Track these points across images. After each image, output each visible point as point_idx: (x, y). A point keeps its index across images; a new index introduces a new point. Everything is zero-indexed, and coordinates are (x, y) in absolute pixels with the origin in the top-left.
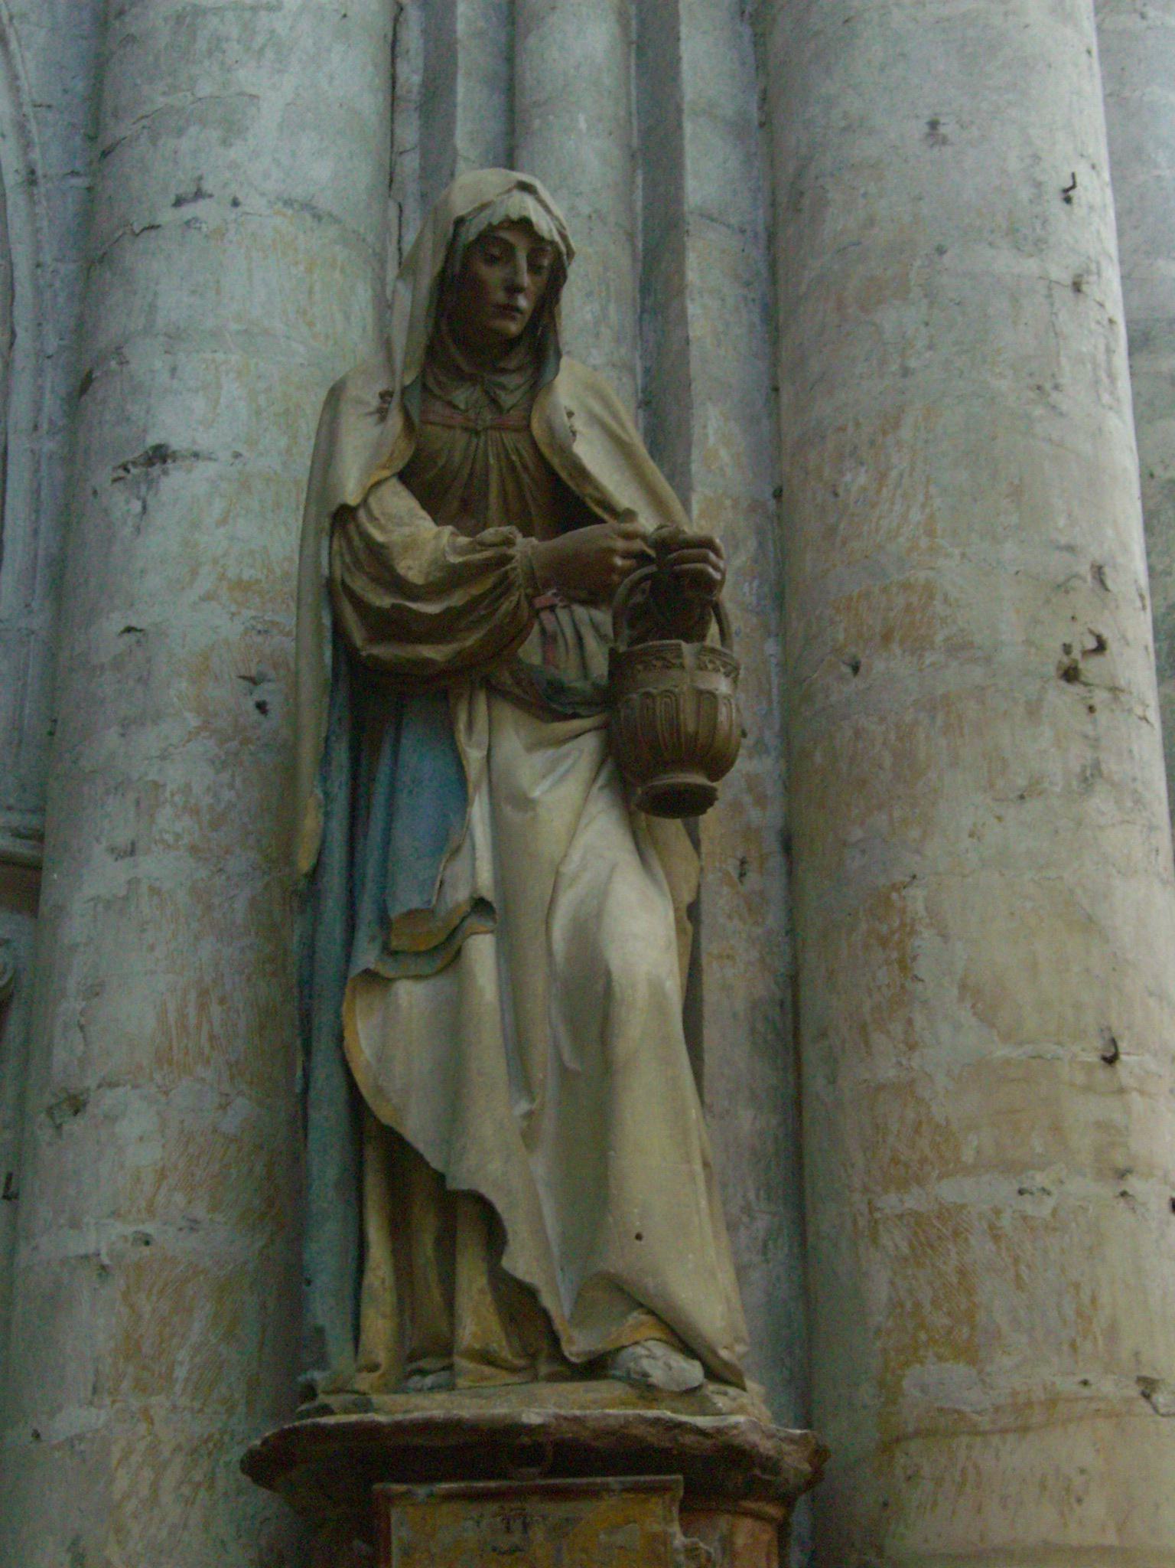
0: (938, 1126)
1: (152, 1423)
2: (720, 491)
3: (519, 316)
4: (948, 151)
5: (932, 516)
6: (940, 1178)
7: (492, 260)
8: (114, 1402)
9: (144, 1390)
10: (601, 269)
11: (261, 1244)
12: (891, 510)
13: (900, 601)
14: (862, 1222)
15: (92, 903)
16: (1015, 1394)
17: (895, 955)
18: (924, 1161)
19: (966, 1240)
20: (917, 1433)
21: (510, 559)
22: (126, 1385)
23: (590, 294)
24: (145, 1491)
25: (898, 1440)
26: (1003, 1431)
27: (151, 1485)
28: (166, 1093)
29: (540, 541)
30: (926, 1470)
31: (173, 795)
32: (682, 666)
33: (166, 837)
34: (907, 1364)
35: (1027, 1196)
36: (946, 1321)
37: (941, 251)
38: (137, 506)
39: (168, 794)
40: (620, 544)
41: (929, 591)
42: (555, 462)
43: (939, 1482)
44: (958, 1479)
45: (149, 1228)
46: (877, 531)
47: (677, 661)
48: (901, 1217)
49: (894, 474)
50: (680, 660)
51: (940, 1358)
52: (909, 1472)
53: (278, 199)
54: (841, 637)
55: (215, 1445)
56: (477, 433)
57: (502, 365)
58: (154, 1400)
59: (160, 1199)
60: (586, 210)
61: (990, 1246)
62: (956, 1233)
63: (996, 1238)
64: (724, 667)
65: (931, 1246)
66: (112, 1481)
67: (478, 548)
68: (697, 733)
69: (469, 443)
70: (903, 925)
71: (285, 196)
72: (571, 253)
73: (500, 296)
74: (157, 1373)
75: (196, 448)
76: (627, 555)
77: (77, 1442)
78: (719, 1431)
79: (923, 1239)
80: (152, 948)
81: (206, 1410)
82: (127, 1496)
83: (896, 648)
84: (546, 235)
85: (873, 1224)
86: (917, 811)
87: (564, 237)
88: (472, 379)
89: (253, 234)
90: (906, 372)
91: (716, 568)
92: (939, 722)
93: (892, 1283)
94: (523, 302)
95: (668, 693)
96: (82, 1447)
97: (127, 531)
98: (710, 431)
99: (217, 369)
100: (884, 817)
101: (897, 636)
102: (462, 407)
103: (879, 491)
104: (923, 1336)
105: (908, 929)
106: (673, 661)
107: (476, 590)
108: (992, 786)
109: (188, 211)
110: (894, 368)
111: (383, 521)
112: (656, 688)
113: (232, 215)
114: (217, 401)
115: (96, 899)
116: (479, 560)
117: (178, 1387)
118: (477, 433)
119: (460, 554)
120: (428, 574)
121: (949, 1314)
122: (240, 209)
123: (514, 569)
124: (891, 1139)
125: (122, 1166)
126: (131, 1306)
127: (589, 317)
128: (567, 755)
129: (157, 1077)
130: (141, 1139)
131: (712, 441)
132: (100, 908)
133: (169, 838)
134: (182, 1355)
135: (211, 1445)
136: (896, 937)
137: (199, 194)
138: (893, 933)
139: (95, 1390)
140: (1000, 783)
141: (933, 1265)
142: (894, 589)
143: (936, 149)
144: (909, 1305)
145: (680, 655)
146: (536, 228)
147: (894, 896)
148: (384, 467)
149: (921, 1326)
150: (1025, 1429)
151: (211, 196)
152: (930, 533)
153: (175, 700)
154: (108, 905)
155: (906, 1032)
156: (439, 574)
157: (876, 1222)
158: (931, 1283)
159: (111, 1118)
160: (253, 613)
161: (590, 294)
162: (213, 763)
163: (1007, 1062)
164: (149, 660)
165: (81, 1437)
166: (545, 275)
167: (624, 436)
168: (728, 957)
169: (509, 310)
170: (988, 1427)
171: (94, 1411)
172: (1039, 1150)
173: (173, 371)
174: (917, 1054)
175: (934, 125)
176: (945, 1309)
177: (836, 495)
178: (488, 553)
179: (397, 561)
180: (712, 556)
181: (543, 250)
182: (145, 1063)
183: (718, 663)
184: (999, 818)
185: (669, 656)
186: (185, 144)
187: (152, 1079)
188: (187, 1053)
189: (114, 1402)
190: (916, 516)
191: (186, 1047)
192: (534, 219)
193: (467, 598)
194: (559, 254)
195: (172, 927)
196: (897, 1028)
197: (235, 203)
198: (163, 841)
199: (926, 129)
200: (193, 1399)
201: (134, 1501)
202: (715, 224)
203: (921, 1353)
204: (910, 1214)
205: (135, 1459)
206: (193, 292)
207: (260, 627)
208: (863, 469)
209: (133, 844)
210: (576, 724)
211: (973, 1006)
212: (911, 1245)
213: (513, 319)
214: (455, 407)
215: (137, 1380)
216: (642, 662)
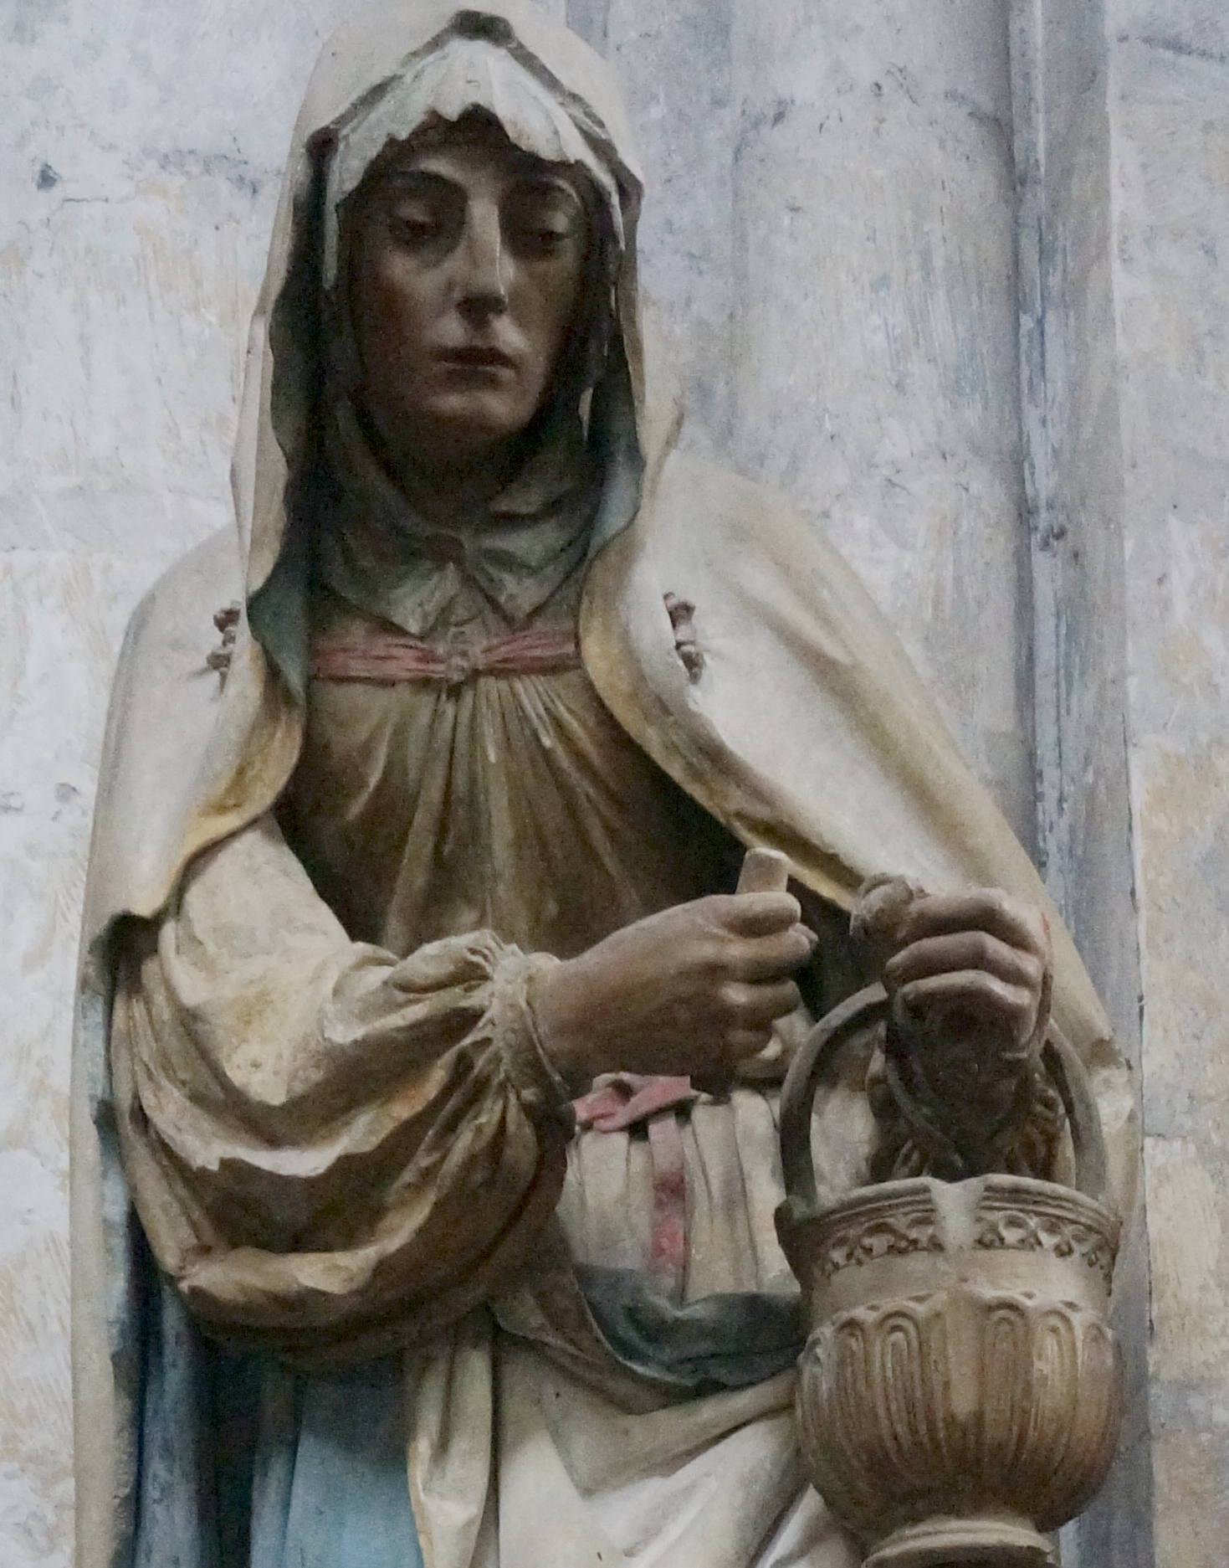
2: (1204, 738)
3: (506, 374)
7: (415, 237)
10: (908, 216)
21: (468, 1018)
23: (881, 283)
29: (563, 955)
32: (937, 1246)
40: (739, 951)
42: (652, 741)
47: (921, 1234)
50: (930, 1230)
53: (147, 152)
56: (455, 692)
57: (503, 505)
60: (865, 71)
64: (1052, 1229)
67: (401, 996)
68: (979, 1417)
69: (436, 714)
71: (165, 145)
72: (629, 188)
73: (452, 331)
76: (760, 975)
84: (547, 152)
87: (603, 148)
88: (441, 553)
89: (88, 250)
91: (1014, 977)
94: (508, 334)
95: (893, 1320)
98: (1178, 585)
102: (414, 627)
106: (913, 1234)
107: (403, 1110)
111: (211, 948)
112: (873, 1308)
113: (42, 204)
116: (399, 1029)
118: (455, 692)
119: (363, 1017)
120: (293, 1077)
122: (57, 192)
123: (487, 1041)
128: (689, 1491)
131: (1181, 609)
145: (928, 1216)
146: (511, 133)
148: (221, 809)
156: (317, 1076)
161: (881, 283)
162: (29, 1532)
166: (567, 259)
167: (833, 650)
178: (417, 1011)
179: (225, 1051)
180: (994, 946)
181: (547, 190)
183: (1033, 1222)
185: (899, 1221)
192: (503, 110)
193: (389, 1127)
194: (595, 198)
197: (47, 179)
202: (1184, 60)
210: (712, 1411)
213: (493, 383)
214: (400, 631)
216: (842, 1242)
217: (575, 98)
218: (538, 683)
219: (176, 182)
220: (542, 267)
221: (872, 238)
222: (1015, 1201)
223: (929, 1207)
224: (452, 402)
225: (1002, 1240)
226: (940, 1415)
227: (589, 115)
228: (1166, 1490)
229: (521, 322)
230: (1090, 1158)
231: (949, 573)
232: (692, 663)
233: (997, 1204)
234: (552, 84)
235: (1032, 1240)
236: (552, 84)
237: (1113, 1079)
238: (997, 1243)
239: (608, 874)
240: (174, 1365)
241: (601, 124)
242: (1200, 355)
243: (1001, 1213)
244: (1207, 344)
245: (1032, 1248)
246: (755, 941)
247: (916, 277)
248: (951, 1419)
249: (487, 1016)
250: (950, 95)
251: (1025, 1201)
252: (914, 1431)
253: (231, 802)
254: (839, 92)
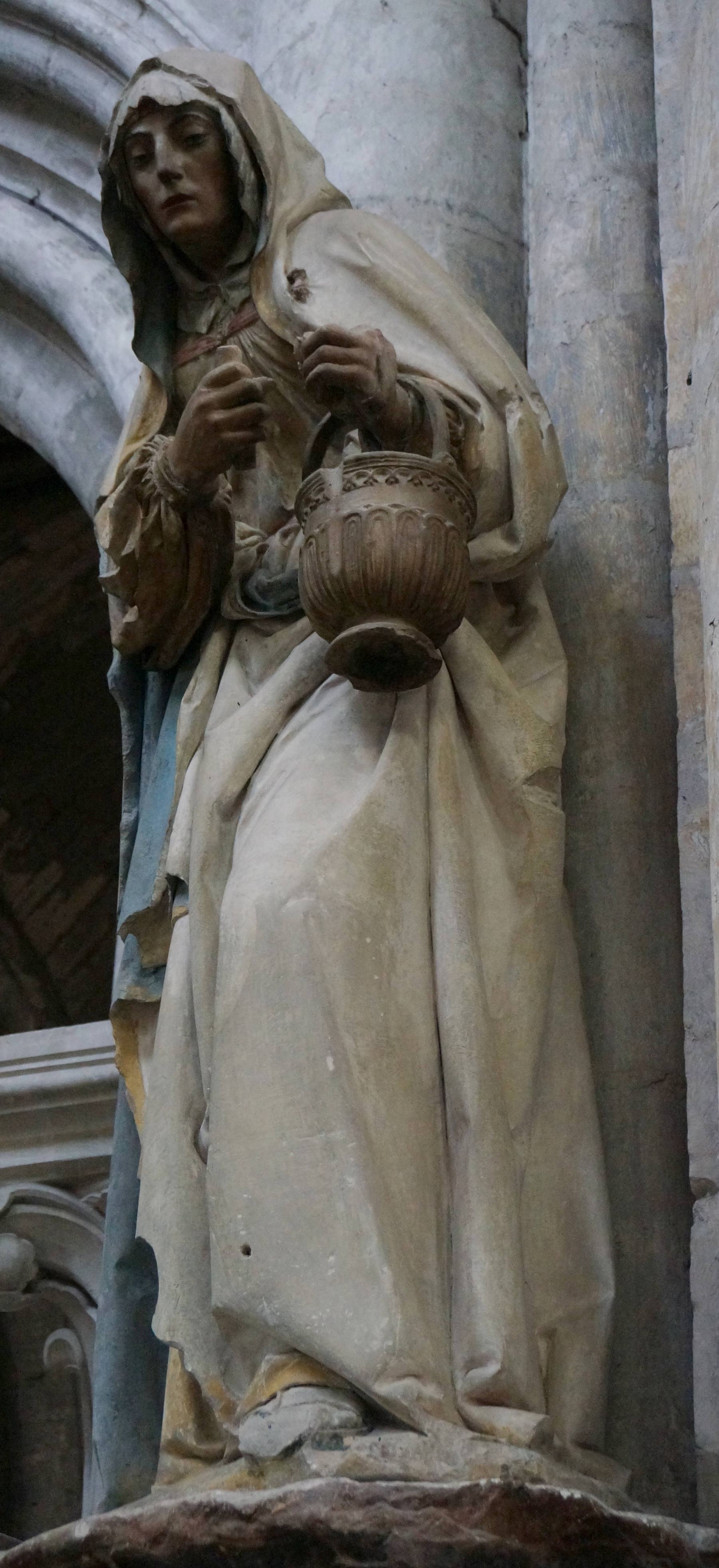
68: (343, 571)
73: (162, 194)
78: (261, 1509)
87: (209, 91)
94: (187, 186)
169: (178, 203)
183: (370, 472)
213: (186, 209)
217: (192, 76)
218: (248, 333)
220: (198, 152)
222: (358, 465)
223: (321, 482)
224: (176, 223)
225: (354, 485)
226: (327, 576)
227: (201, 80)
228: (680, 620)
229: (194, 178)
231: (598, 232)
233: (351, 469)
234: (181, 74)
235: (371, 481)
236: (181, 74)
237: (512, 408)
238: (353, 487)
239: (289, 403)
240: (152, 691)
241: (205, 81)
243: (354, 473)
245: (371, 484)
246: (222, 389)
247: (583, 107)
248: (331, 577)
249: (149, 470)
250: (603, 22)
251: (366, 463)
252: (320, 590)
253: (141, 434)
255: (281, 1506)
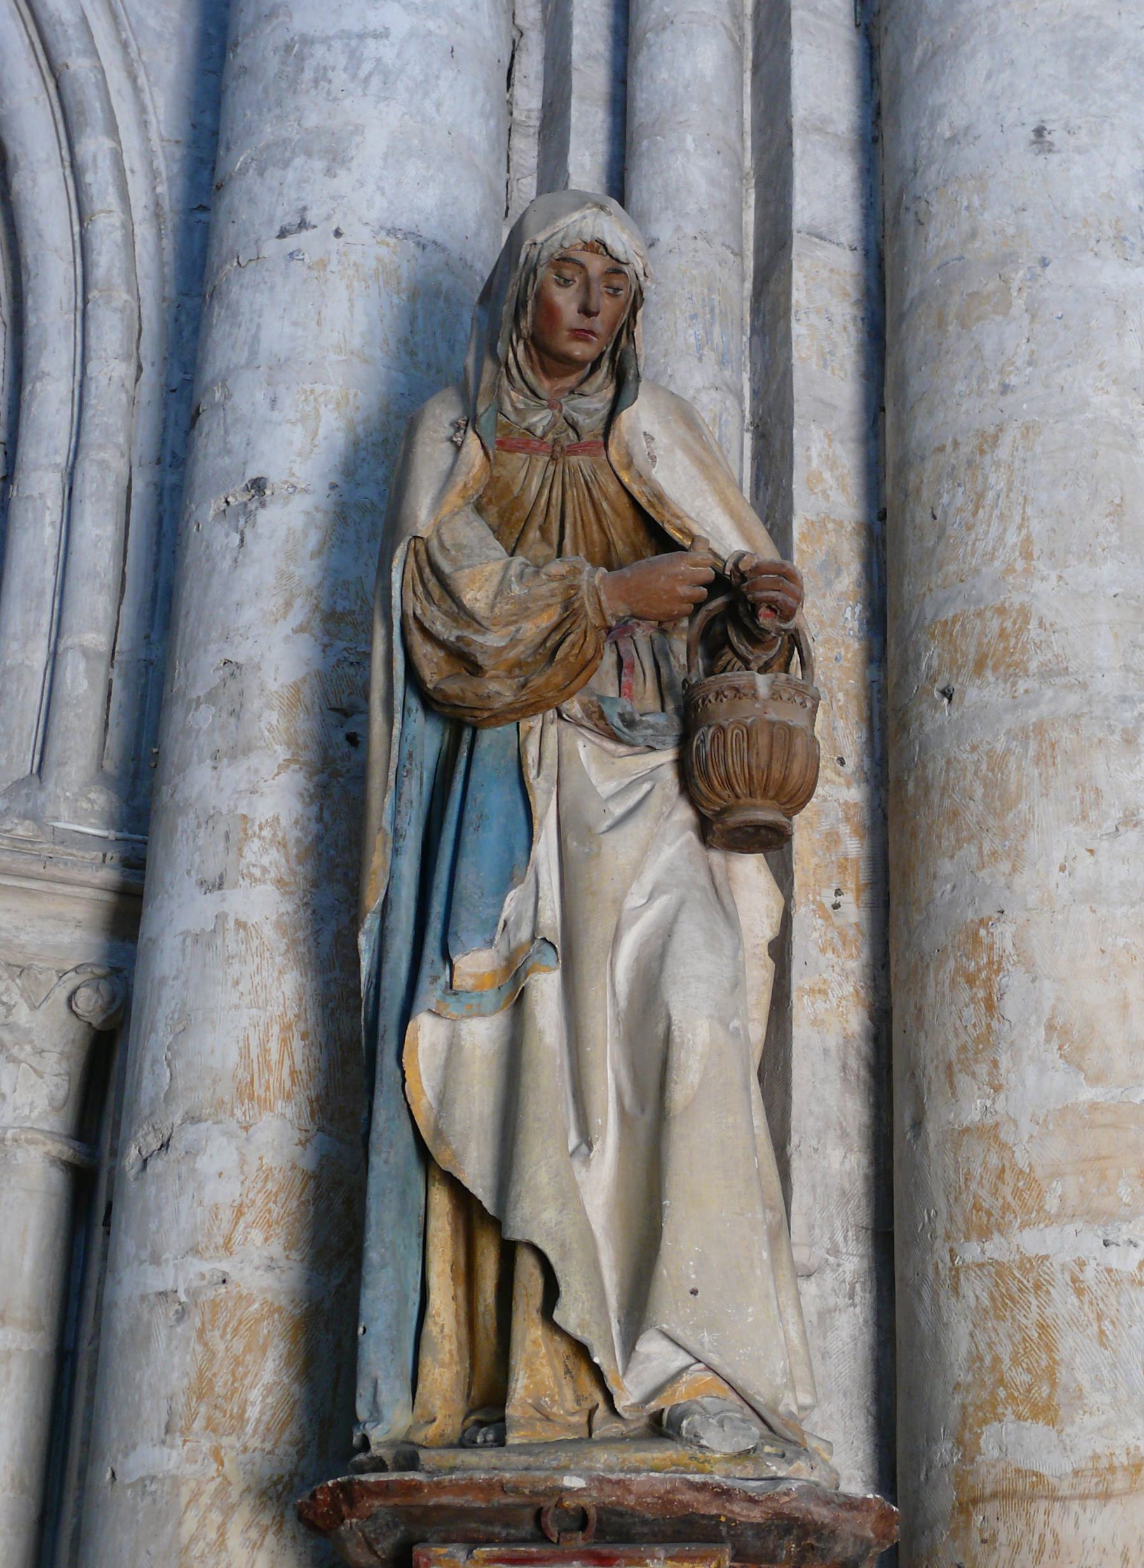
0: (1021, 1172)
1: (222, 1464)
4: (1055, 159)
5: (1028, 540)
6: (1022, 1227)
8: (185, 1441)
9: (214, 1431)
11: (336, 1281)
12: (986, 533)
13: (995, 625)
14: (944, 1273)
15: (181, 938)
16: (1096, 1457)
17: (981, 994)
18: (1006, 1207)
19: (1048, 1292)
20: (994, 1495)
22: (198, 1425)
23: (694, 317)
24: (212, 1535)
25: (975, 1501)
26: (1084, 1497)
27: (219, 1528)
28: (246, 1129)
30: (1002, 1537)
31: (261, 829)
33: (253, 870)
34: (985, 1421)
35: (1113, 1247)
36: (1027, 1378)
37: (1044, 263)
38: (236, 538)
39: (256, 828)
41: (1024, 614)
42: (635, 489)
43: (1016, 1548)
44: (1035, 1546)
45: (225, 1266)
46: (973, 553)
48: (981, 1266)
49: (990, 495)
51: (1019, 1417)
52: (986, 1535)
53: (381, 228)
54: (935, 663)
55: (284, 1488)
58: (226, 1441)
59: (238, 1237)
61: (1073, 1299)
62: (1038, 1287)
63: (1080, 1292)
65: (1012, 1299)
66: (180, 1524)
70: (990, 962)
71: (389, 225)
74: (228, 1414)
75: (293, 480)
77: (148, 1482)
79: (1004, 1291)
80: (237, 983)
81: (276, 1451)
82: (193, 1539)
83: (989, 675)
85: (953, 1273)
86: (1007, 843)
89: (355, 264)
90: (1005, 389)
92: (1031, 753)
93: (971, 1335)
96: (153, 1487)
97: (226, 564)
99: (315, 399)
100: (974, 850)
101: (990, 663)
103: (975, 514)
104: (1002, 1393)
105: (995, 967)
108: (1084, 817)
109: (291, 242)
110: (993, 385)
114: (315, 434)
115: (186, 934)
117: (249, 1429)
121: (1029, 1371)
124: (973, 1186)
125: (201, 1203)
126: (206, 1345)
127: (692, 340)
129: (238, 1112)
130: (220, 1175)
131: (815, 463)
132: (189, 941)
133: (257, 872)
134: (255, 1395)
135: (280, 1488)
136: (983, 975)
137: (303, 225)
138: (979, 971)
139: (168, 1430)
140: (1093, 815)
141: (1013, 1318)
142: (989, 614)
143: (1041, 157)
144: (988, 1360)
145: (753, 687)
147: (983, 932)
149: (1001, 1382)
150: (1106, 1496)
151: (315, 227)
152: (1027, 555)
153: (266, 733)
154: (196, 939)
155: (990, 1074)
157: (957, 1270)
158: (1010, 1337)
159: (191, 1153)
160: (345, 644)
161: (694, 317)
163: (1094, 1106)
164: (241, 693)
165: (153, 1479)
168: (820, 991)
170: (1068, 1493)
171: (166, 1450)
172: (1126, 1200)
173: (274, 401)
174: (1002, 1096)
175: (1039, 132)
176: (1025, 1366)
177: (935, 517)
182: (227, 1098)
184: (1091, 852)
186: (291, 175)
187: (233, 1115)
188: (268, 1088)
189: (185, 1441)
190: (1012, 538)
191: (268, 1082)
195: (257, 960)
196: (982, 1069)
197: (338, 233)
198: (251, 875)
199: (1032, 137)
200: (263, 1441)
201: (201, 1544)
203: (1000, 1410)
204: (991, 1264)
205: (205, 1500)
206: (295, 324)
207: (352, 659)
208: (961, 490)
209: (221, 877)
211: (1060, 1048)
212: (992, 1298)
215: (209, 1419)
219: (392, 241)
221: (691, 298)
230: (808, 672)
232: (653, 459)
242: (825, 360)
244: (828, 357)
247: (708, 316)
254: (328, 170)
255: (787, 1499)
